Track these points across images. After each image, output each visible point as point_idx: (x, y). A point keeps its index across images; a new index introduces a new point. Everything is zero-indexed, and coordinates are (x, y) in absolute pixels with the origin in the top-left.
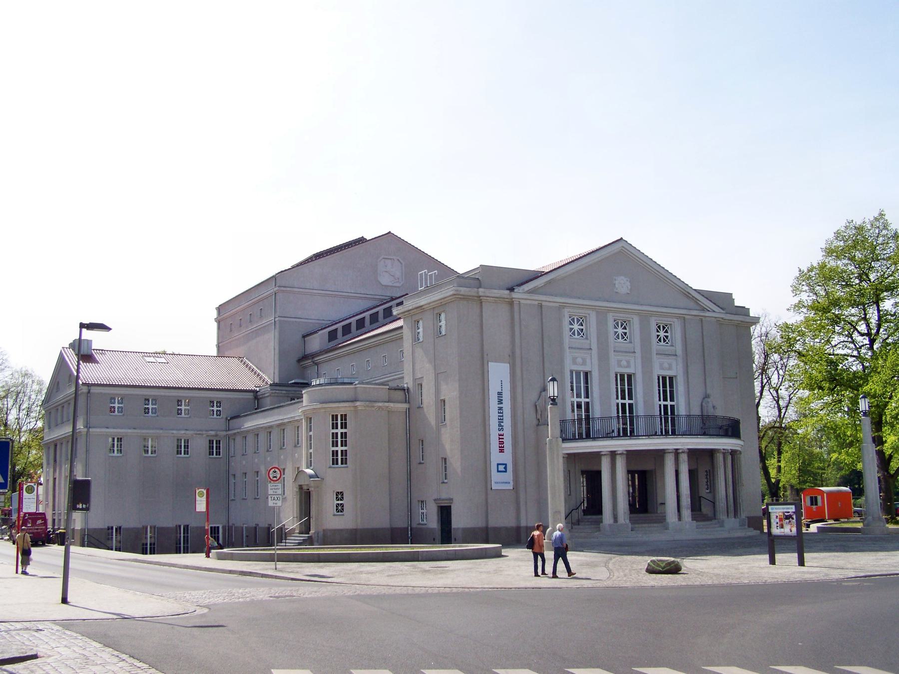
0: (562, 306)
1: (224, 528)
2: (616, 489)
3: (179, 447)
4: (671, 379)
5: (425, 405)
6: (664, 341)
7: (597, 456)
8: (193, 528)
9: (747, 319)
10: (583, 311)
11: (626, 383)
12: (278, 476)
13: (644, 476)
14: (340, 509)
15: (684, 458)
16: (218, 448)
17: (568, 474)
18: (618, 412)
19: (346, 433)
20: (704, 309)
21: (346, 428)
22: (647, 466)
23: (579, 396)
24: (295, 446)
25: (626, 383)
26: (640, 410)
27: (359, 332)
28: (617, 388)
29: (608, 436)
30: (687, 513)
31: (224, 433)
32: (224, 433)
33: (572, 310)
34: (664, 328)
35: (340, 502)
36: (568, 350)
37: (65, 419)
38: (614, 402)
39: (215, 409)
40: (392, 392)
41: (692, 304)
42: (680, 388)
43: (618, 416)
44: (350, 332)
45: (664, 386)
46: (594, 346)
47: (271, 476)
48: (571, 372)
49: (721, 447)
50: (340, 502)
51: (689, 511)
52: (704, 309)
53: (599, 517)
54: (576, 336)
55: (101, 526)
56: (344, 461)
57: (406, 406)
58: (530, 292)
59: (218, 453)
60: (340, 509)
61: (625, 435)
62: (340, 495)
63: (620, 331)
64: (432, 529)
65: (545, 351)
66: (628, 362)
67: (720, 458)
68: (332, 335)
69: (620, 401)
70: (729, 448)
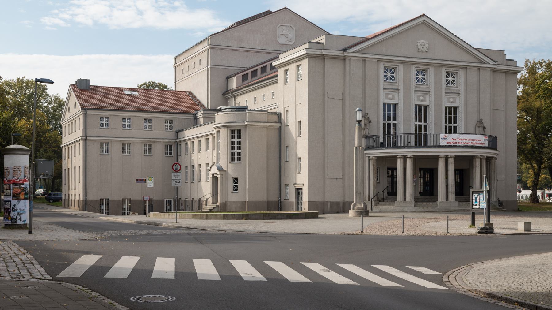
0: (380, 61)
1: (175, 201)
2: (446, 179)
3: (129, 149)
4: (455, 109)
5: (290, 124)
6: (391, 79)
7: (394, 159)
8: (155, 200)
9: (515, 69)
10: (394, 64)
11: (422, 111)
12: (179, 168)
13: (427, 171)
14: (236, 189)
15: (451, 161)
16: (171, 150)
17: (377, 171)
18: (416, 130)
19: (240, 142)
20: (482, 62)
21: (240, 138)
22: (464, 166)
23: (420, 121)
24: (206, 151)
25: (422, 111)
26: (401, 129)
27: (262, 75)
28: (446, 117)
29: (408, 146)
30: (452, 197)
31: (174, 141)
32: (174, 141)
33: (386, 63)
34: (391, 70)
35: (236, 184)
36: (413, 92)
37: (73, 131)
38: (382, 122)
39: (169, 125)
40: (270, 116)
41: (471, 59)
42: (461, 115)
43: (416, 133)
44: (256, 75)
45: (450, 114)
46: (401, 87)
47: (174, 168)
48: (384, 104)
49: (479, 155)
50: (236, 184)
51: (454, 195)
52: (482, 62)
53: (312, 200)
54: (389, 81)
55: (96, 199)
56: (239, 159)
57: (278, 125)
58: (358, 52)
59: (171, 153)
60: (236, 189)
61: (389, 145)
62: (235, 180)
63: (450, 79)
64: (292, 202)
65: (366, 91)
66: (393, 96)
67: (478, 161)
68: (245, 77)
69: (448, 125)
70: (485, 155)
